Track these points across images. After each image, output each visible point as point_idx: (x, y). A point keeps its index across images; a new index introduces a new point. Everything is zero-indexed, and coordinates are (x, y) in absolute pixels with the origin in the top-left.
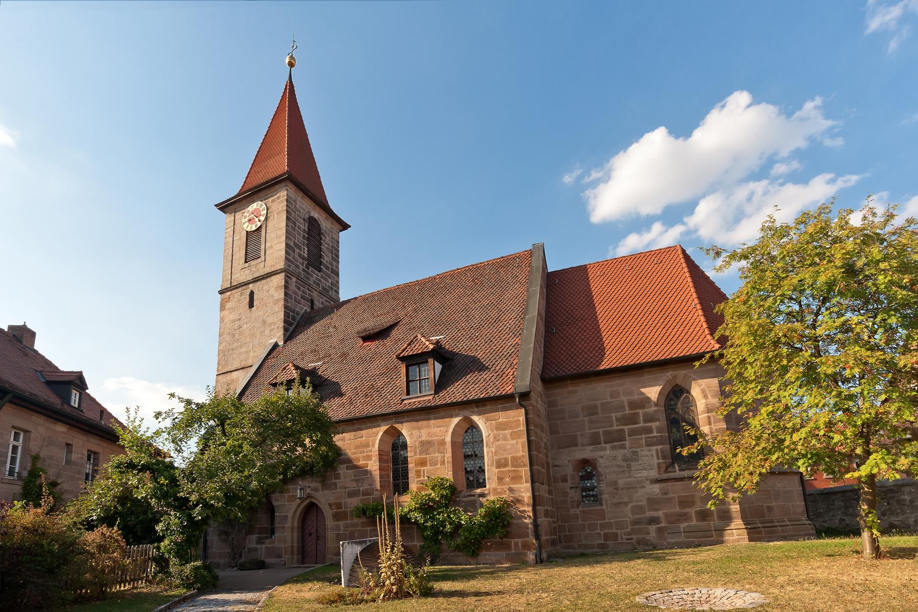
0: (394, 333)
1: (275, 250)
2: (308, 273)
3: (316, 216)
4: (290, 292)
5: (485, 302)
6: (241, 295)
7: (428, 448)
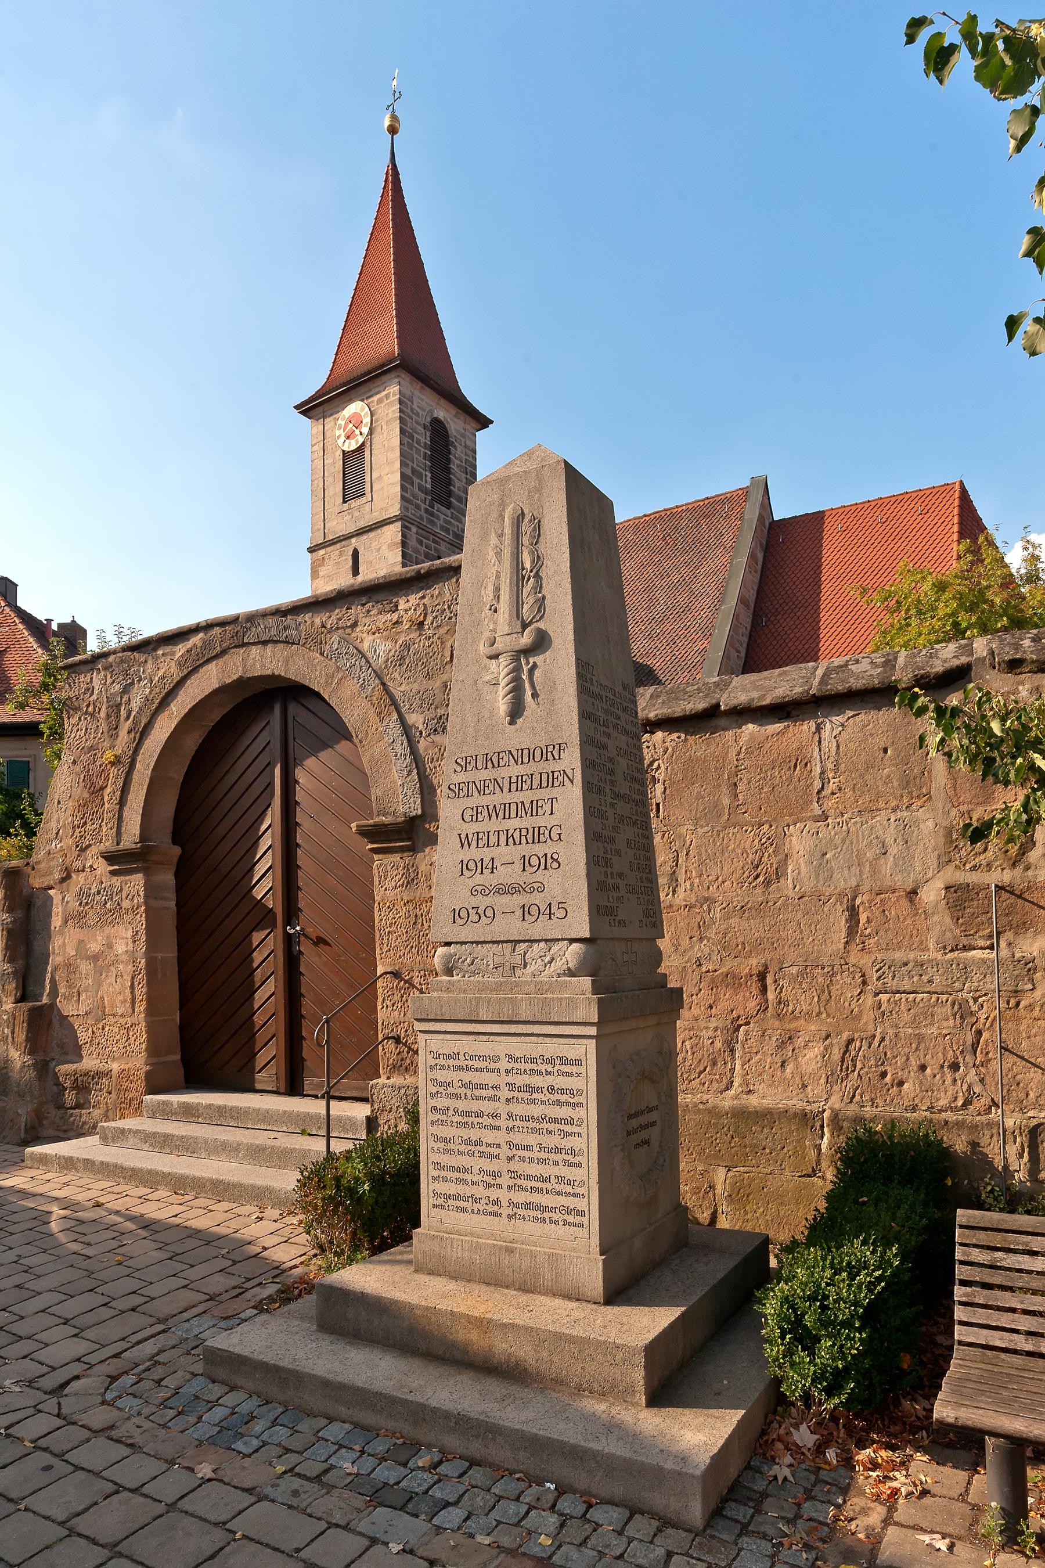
2: (432, 514)
3: (441, 414)
5: (675, 578)
6: (341, 555)
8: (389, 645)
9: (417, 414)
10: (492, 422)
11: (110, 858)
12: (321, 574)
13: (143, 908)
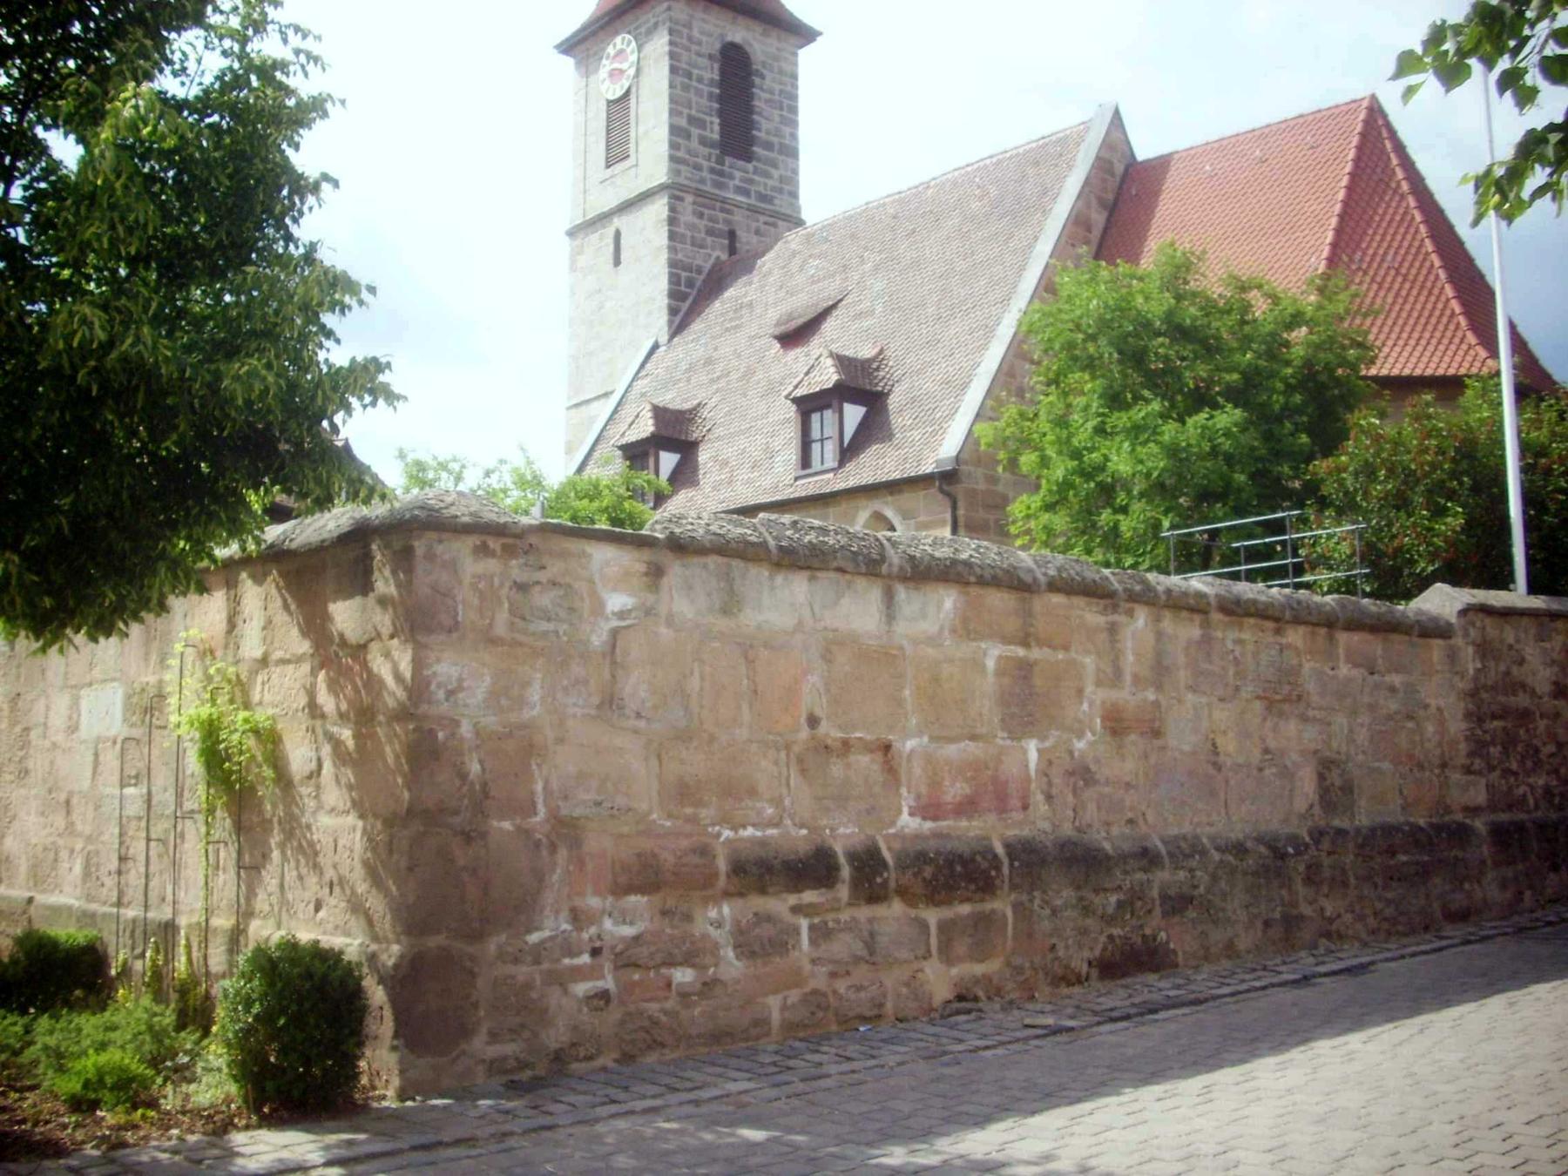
0: (829, 326)
2: (721, 174)
3: (299, 754)
4: (681, 230)
9: (700, 43)
10: (820, 34)
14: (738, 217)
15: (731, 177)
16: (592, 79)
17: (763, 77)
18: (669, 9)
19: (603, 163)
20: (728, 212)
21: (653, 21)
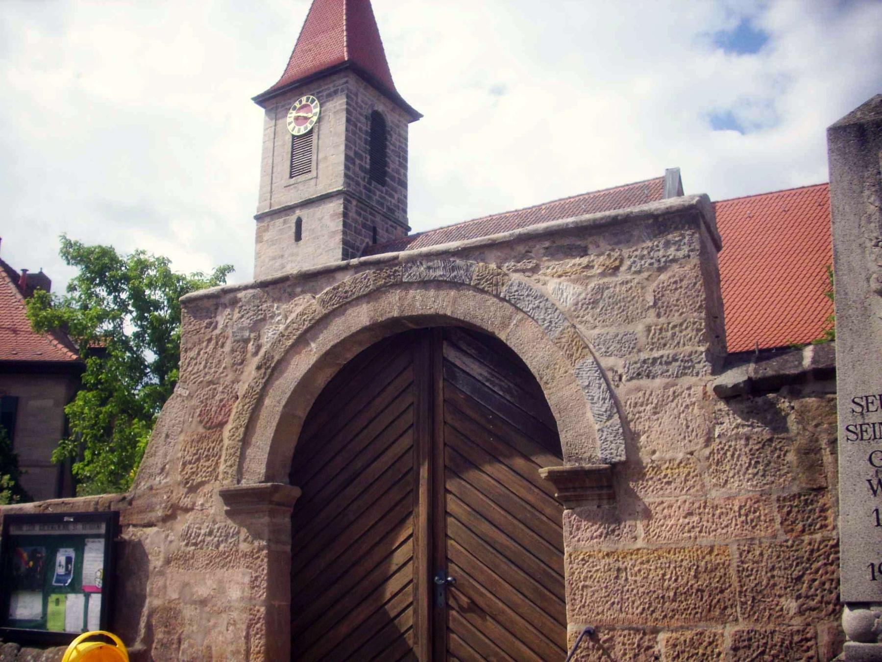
1: (331, 167)
2: (370, 191)
3: (380, 108)
4: (349, 221)
7: (679, 246)
8: (579, 288)
9: (361, 107)
10: (421, 116)
11: (228, 497)
12: (265, 239)
13: (265, 552)
14: (378, 218)
15: (375, 194)
16: (280, 122)
17: (391, 135)
18: (347, 82)
19: (288, 175)
20: (374, 216)
21: (332, 90)
